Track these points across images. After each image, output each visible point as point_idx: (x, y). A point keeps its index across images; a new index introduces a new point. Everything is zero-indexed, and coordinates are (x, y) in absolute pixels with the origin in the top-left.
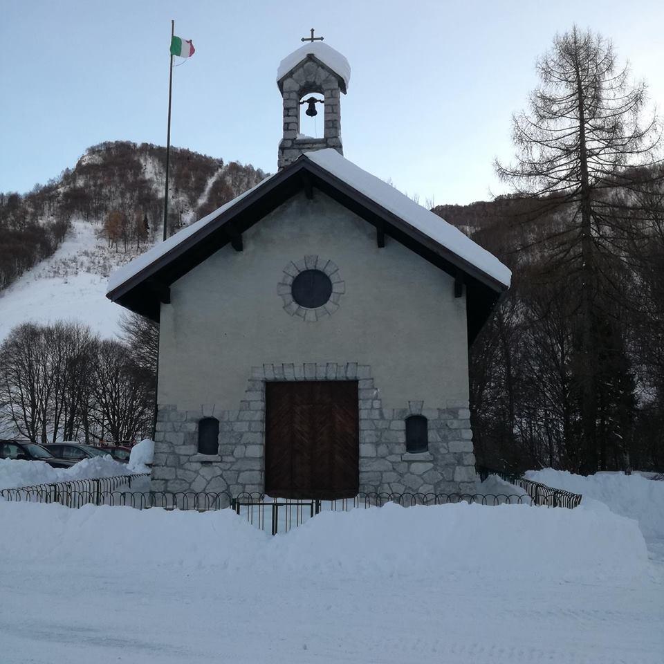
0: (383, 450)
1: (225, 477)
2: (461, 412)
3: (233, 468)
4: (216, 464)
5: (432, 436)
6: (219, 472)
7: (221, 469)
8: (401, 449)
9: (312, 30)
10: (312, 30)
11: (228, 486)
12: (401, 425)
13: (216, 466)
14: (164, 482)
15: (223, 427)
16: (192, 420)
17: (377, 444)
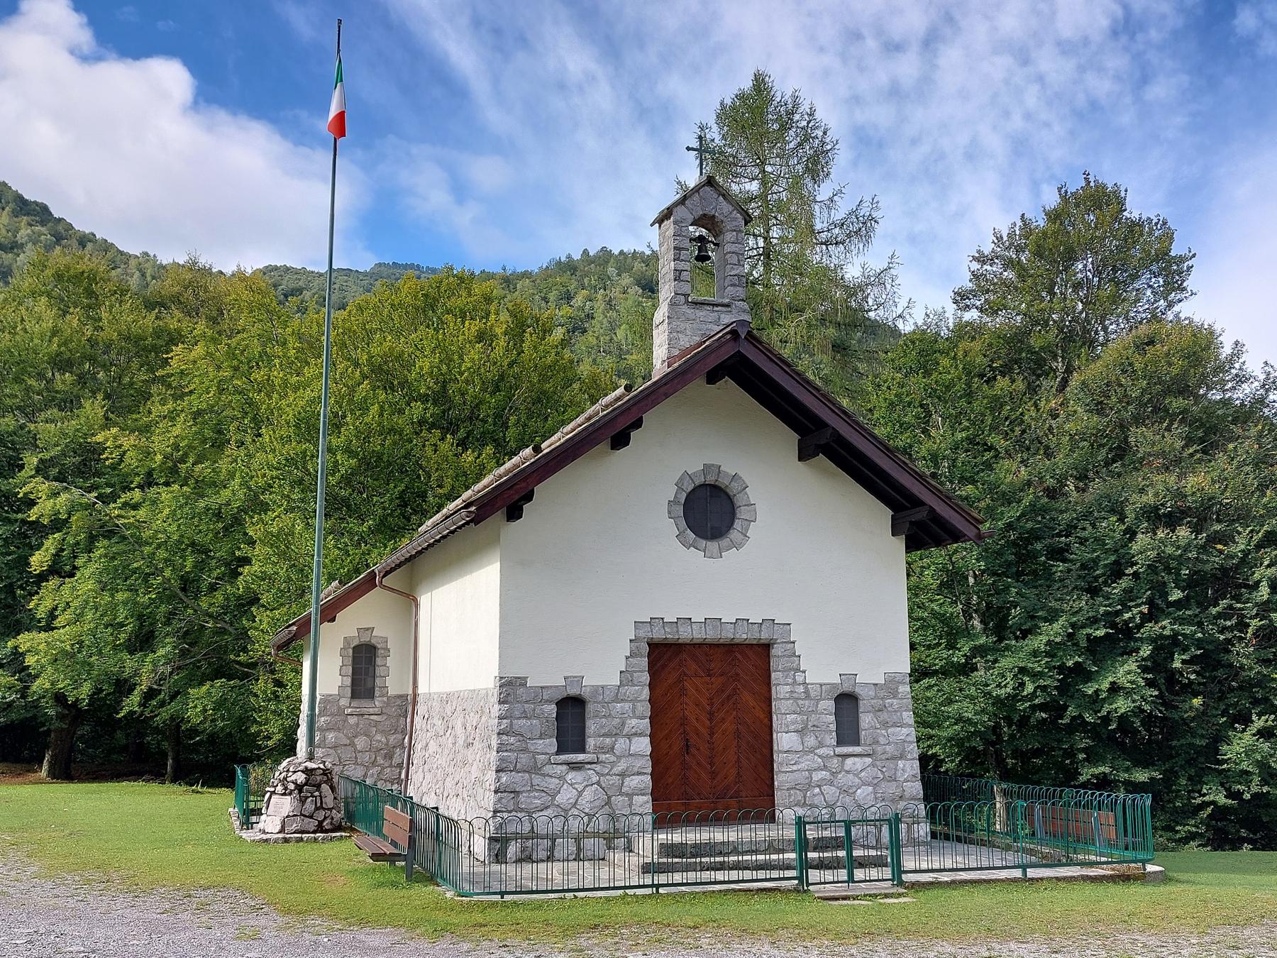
0: (811, 741)
1: (604, 785)
2: (901, 689)
3: (615, 770)
4: (589, 766)
5: (866, 720)
6: (595, 779)
7: (597, 773)
8: (831, 739)
9: (688, 149)
10: (688, 149)
11: (609, 798)
12: (830, 705)
13: (589, 769)
14: (513, 795)
15: (590, 708)
16: (549, 702)
17: (801, 732)
